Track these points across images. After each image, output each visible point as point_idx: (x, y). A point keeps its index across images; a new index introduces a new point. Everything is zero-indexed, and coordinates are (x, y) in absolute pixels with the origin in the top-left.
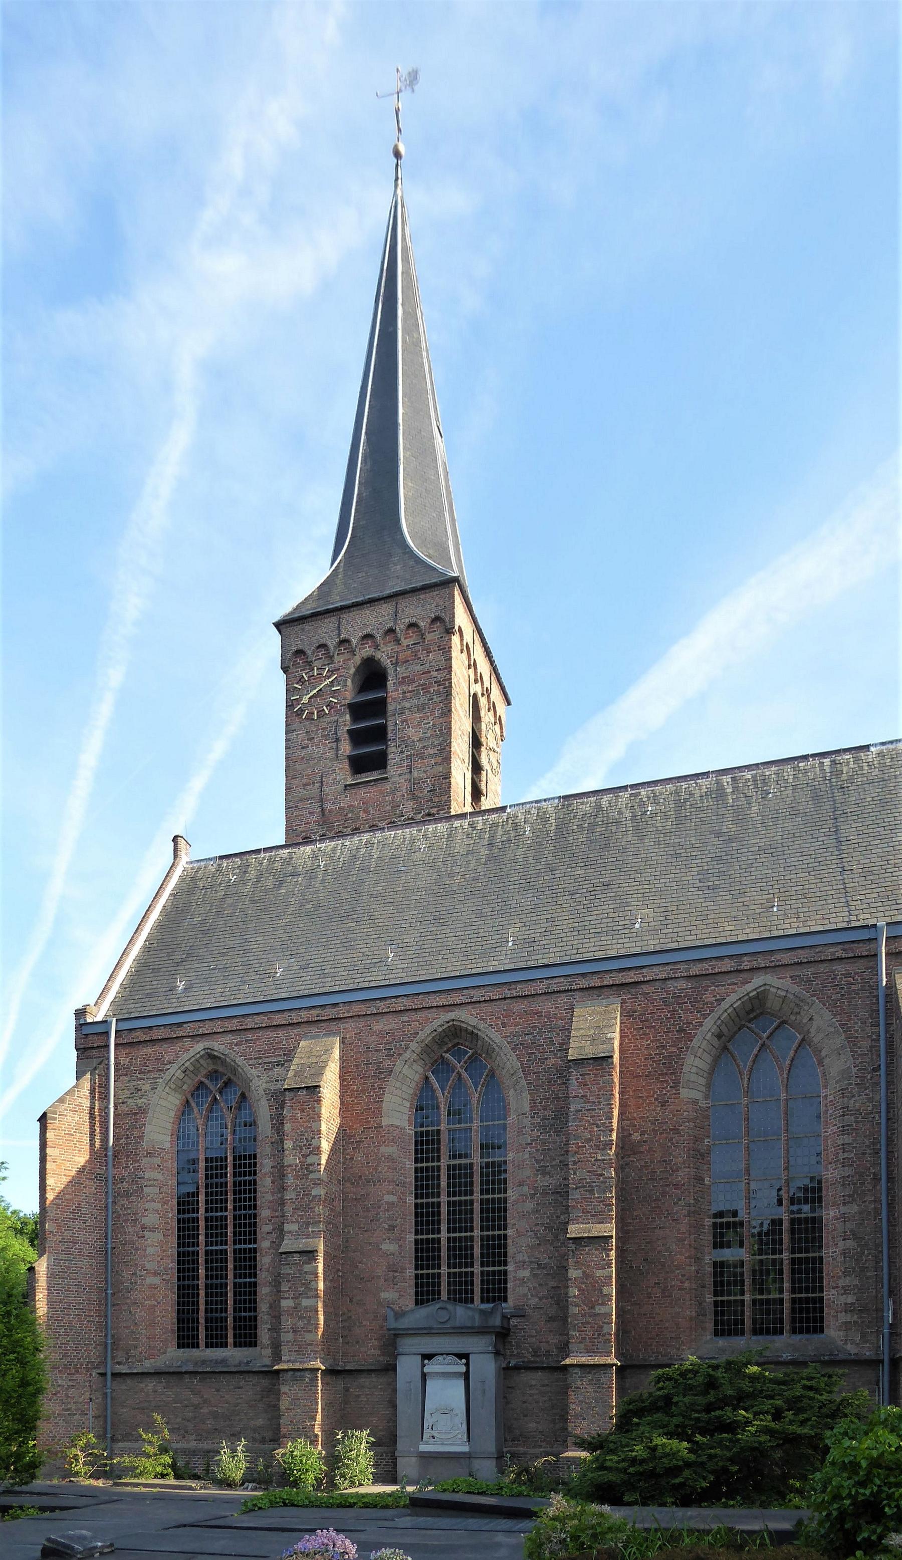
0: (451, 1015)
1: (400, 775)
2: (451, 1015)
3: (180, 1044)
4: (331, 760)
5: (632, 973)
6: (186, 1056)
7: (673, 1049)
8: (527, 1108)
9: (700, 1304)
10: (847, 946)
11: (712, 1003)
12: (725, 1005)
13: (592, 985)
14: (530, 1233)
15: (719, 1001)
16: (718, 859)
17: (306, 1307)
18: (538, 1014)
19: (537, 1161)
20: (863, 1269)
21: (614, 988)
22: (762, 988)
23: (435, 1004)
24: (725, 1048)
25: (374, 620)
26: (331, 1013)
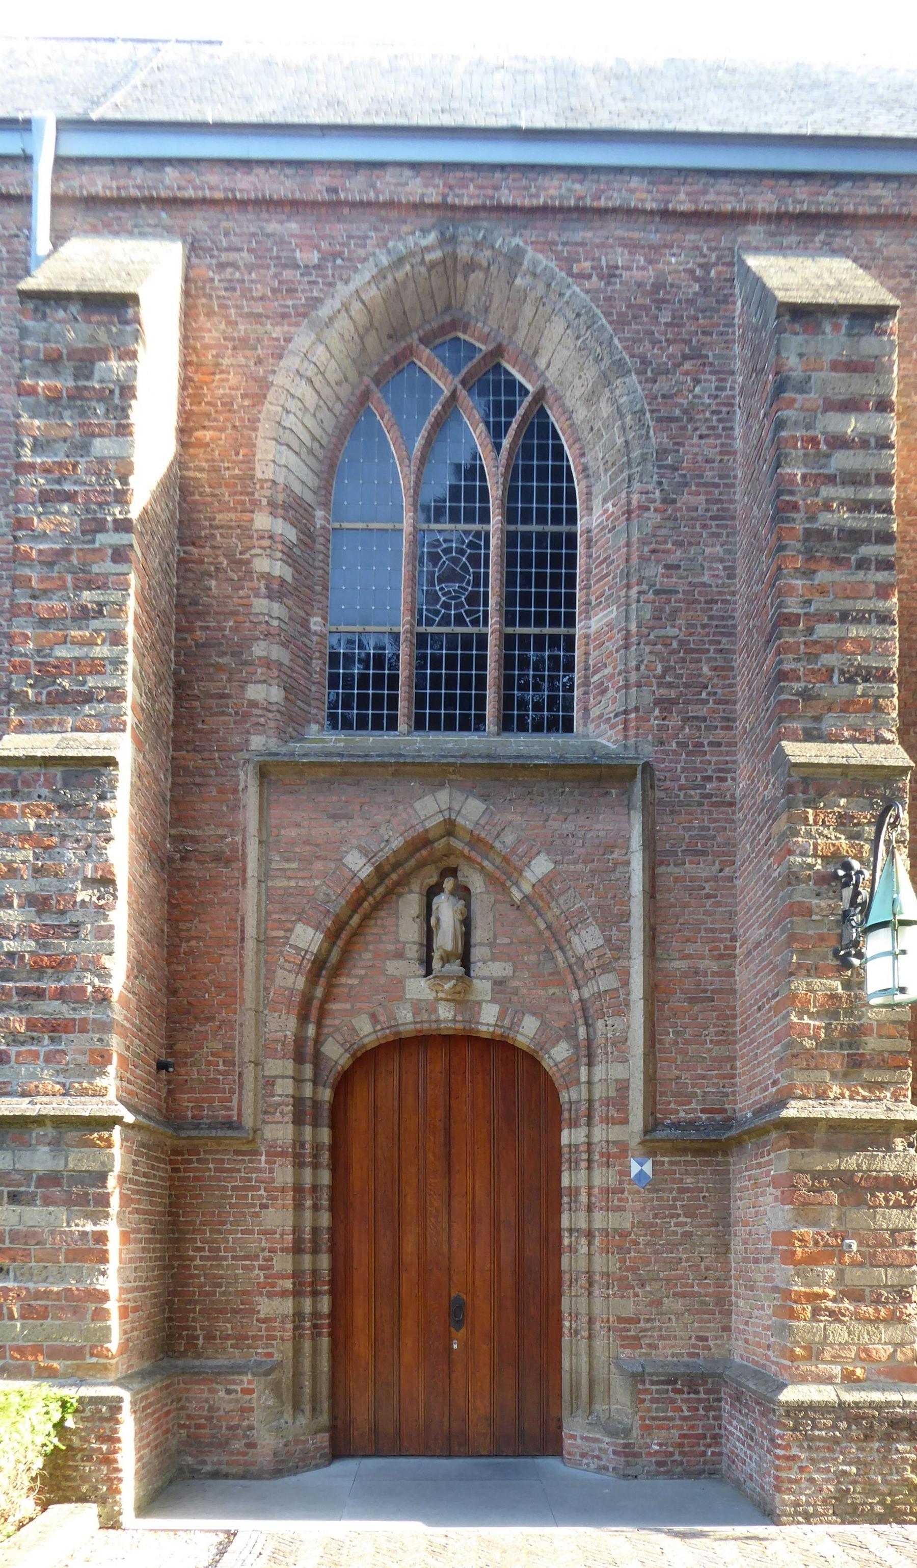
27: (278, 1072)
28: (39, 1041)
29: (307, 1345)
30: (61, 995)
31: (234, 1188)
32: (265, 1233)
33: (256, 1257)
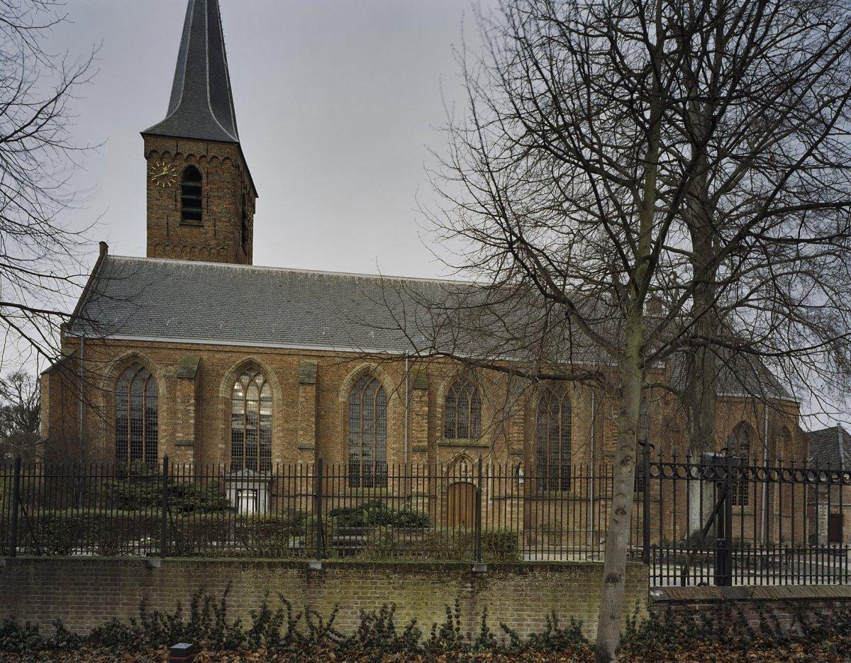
0: (250, 356)
2: (250, 356)
12: (355, 370)
24: (355, 386)
25: (199, 149)
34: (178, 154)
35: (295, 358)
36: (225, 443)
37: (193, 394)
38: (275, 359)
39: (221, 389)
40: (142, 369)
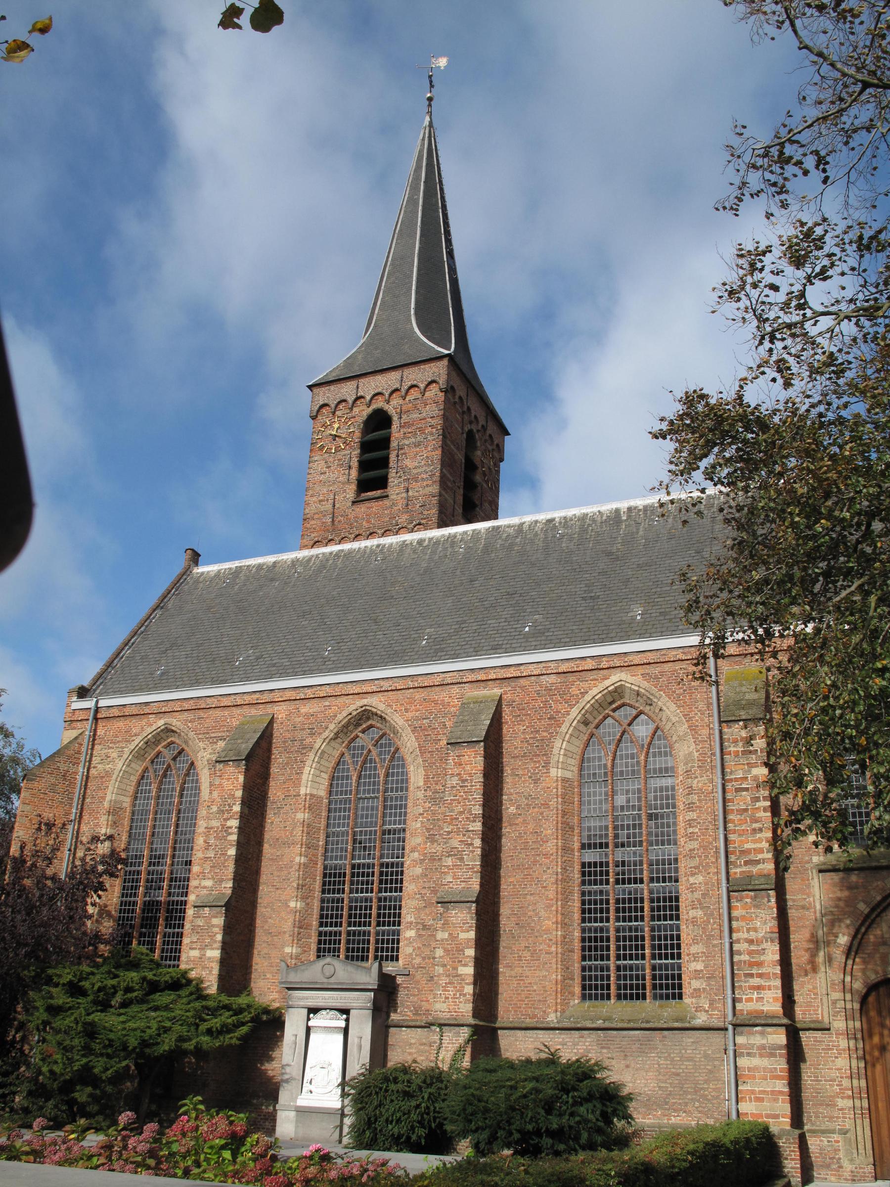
1: (398, 494)
2: (365, 702)
3: (146, 720)
4: (343, 484)
5: (512, 669)
6: (149, 730)
7: (545, 734)
8: (421, 783)
9: (568, 968)
10: (686, 650)
11: (577, 695)
12: (588, 697)
13: (480, 678)
14: (418, 896)
15: (584, 694)
16: (603, 573)
17: (210, 958)
18: (435, 702)
19: (428, 830)
20: (710, 937)
21: (498, 682)
22: (619, 684)
23: (352, 692)
26: (266, 697)
27: (837, 998)
28: (753, 993)
29: (859, 1122)
30: (760, 976)
31: (823, 1049)
32: (838, 1069)
33: (835, 1081)
34: (358, 398)
35: (456, 689)
36: (303, 898)
37: (239, 794)
38: (411, 701)
39: (304, 777)
40: (180, 753)
